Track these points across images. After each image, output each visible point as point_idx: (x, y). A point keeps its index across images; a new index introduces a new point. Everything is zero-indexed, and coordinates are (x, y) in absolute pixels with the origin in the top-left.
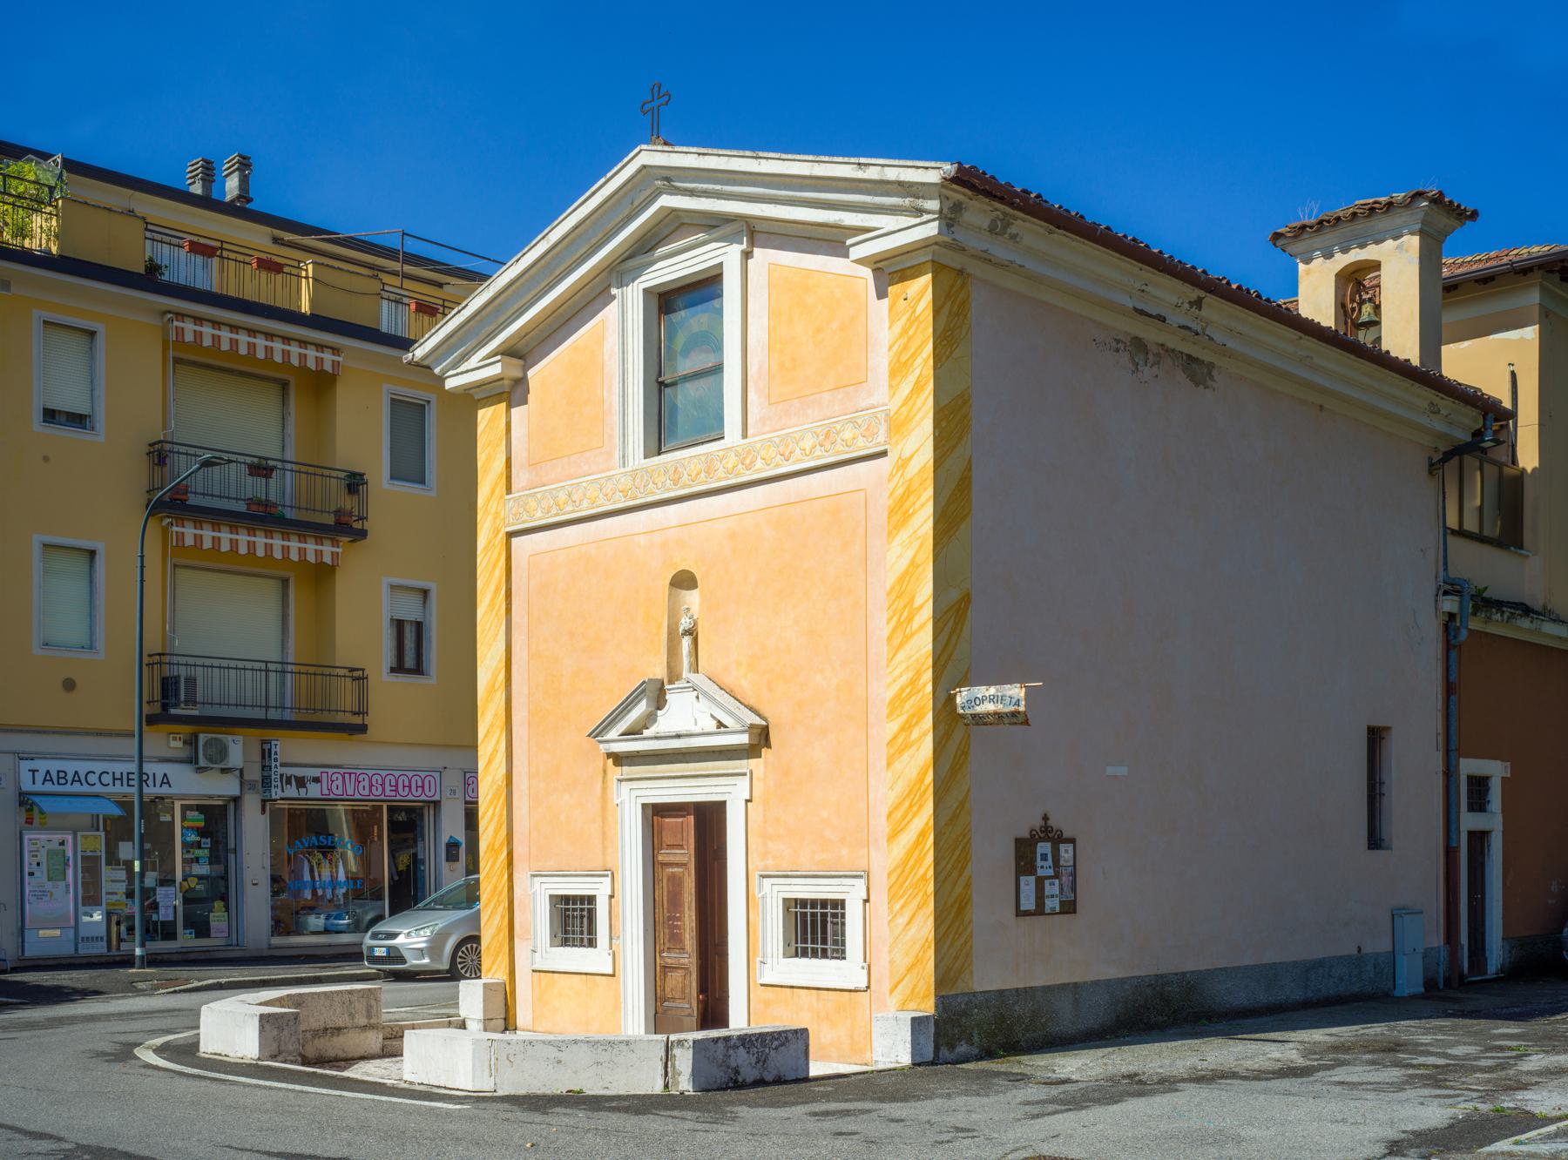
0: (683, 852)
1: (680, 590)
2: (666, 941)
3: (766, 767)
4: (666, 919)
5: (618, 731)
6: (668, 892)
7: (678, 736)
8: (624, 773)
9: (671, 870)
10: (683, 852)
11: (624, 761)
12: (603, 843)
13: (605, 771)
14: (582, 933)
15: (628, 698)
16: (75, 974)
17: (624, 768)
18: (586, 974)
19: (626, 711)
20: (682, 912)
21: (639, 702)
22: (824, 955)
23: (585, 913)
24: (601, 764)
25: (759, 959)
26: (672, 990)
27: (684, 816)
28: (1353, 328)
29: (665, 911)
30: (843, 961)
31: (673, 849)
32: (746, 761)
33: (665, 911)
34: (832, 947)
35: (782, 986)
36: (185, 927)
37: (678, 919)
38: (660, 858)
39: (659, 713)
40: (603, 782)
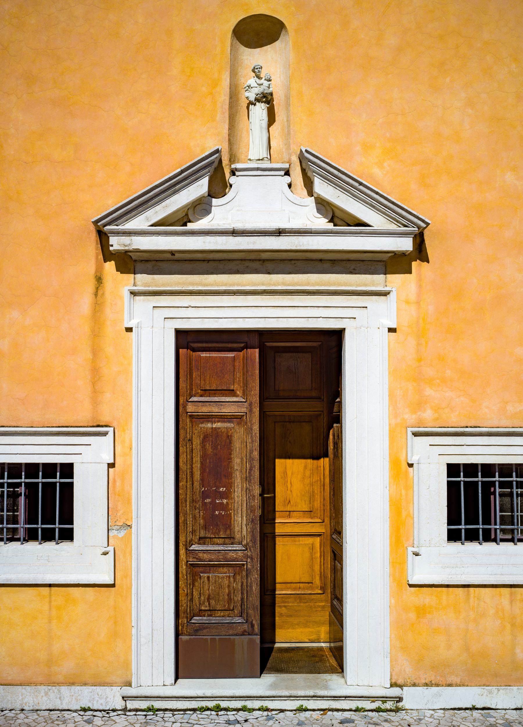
0: (235, 399)
1: (241, 45)
2: (197, 527)
3: (420, 287)
4: (198, 496)
5: (147, 219)
6: (204, 457)
7: (279, 232)
8: (138, 283)
9: (209, 425)
10: (235, 399)
11: (139, 266)
12: (94, 384)
13: (99, 280)
14: (14, 520)
15: (182, 172)
16: (399, 209)
17: (139, 276)
18: (50, 586)
19: (169, 192)
20: (229, 486)
21: (196, 179)
22: (488, 537)
23: (22, 490)
24: (91, 269)
25: (410, 549)
26: (209, 599)
27: (240, 350)
28: (212, 169)
29: (197, 484)
30: (65, 545)
31: (214, 395)
32: (382, 276)
33: (197, 484)
34: (5, 533)
35: (448, 586)
36: (186, 226)
37: (223, 496)
38: (190, 408)
39: (215, 201)
40: (96, 295)
